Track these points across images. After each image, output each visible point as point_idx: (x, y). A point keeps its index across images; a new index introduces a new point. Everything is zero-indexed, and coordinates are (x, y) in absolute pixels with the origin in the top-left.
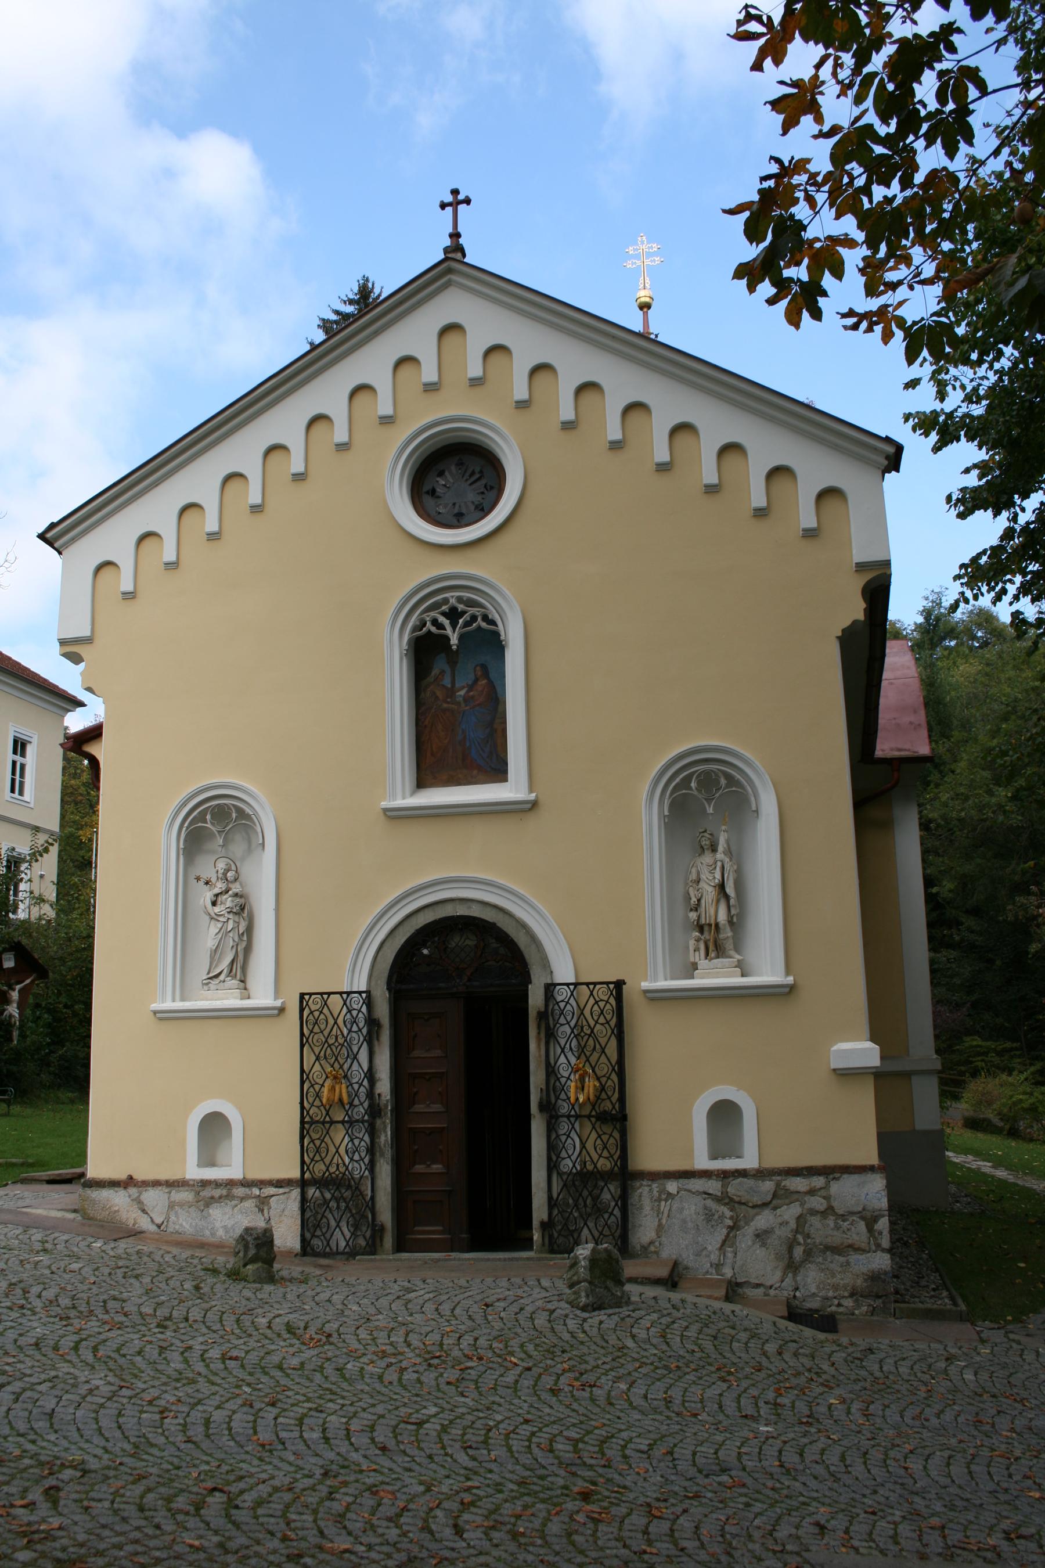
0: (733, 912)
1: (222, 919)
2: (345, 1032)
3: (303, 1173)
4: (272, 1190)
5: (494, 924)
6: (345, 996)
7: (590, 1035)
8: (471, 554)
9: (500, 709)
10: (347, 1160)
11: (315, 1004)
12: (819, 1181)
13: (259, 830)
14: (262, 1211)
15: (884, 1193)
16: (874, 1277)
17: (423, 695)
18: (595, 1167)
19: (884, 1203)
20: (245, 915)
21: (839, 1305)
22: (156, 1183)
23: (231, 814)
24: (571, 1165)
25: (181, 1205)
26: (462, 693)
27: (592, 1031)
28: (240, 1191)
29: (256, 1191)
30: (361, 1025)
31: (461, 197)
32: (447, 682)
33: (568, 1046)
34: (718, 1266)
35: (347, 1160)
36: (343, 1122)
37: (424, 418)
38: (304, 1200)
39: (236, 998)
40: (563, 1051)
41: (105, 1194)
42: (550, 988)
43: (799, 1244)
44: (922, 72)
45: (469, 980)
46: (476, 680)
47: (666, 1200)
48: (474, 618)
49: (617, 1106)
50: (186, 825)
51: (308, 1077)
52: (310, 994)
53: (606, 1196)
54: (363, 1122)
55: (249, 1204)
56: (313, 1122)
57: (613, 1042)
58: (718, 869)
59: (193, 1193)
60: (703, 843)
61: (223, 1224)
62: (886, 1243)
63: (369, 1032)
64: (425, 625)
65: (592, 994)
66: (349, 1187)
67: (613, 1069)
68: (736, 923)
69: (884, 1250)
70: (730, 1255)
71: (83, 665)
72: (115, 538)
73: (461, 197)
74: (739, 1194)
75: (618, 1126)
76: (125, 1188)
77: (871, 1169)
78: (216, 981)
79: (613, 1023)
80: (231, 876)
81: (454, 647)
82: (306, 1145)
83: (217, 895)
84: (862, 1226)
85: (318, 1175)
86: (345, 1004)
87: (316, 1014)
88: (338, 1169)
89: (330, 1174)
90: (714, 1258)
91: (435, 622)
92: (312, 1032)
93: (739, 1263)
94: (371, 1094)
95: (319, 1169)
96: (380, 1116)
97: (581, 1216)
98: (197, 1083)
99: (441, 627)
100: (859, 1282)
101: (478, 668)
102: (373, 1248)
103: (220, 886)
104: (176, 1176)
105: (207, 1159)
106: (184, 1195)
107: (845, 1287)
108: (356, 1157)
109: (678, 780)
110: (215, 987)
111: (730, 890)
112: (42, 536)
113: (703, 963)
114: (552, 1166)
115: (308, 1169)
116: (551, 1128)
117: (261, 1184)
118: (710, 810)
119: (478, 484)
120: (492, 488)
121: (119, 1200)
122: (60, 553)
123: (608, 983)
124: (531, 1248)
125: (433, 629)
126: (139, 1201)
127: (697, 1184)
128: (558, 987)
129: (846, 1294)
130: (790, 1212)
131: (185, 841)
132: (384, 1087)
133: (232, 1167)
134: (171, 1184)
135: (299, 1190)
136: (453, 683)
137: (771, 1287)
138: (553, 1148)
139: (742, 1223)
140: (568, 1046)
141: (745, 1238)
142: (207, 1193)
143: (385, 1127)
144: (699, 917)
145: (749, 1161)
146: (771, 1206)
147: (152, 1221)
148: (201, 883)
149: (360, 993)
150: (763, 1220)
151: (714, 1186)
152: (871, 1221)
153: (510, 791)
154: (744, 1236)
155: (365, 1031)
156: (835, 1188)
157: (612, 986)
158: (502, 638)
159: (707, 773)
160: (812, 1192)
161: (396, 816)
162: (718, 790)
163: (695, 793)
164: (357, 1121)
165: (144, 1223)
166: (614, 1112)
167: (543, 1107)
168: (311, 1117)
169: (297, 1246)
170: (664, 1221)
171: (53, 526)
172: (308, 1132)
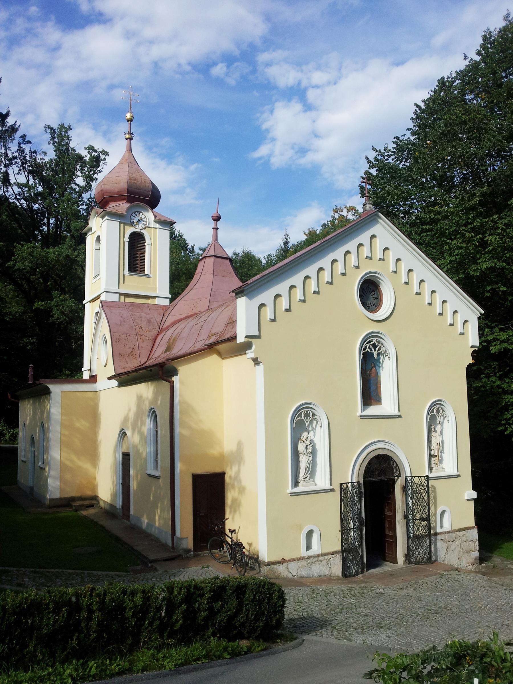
2: (414, 507)
4: (331, 556)
11: (344, 486)
22: (294, 560)
28: (321, 558)
29: (326, 557)
41: (275, 567)
44: (492, 354)
62: (478, 549)
77: (474, 527)
99: (371, 350)
104: (298, 556)
106: (303, 563)
117: (329, 554)
133: (316, 549)
142: (311, 560)
150: (453, 546)
169: (340, 575)
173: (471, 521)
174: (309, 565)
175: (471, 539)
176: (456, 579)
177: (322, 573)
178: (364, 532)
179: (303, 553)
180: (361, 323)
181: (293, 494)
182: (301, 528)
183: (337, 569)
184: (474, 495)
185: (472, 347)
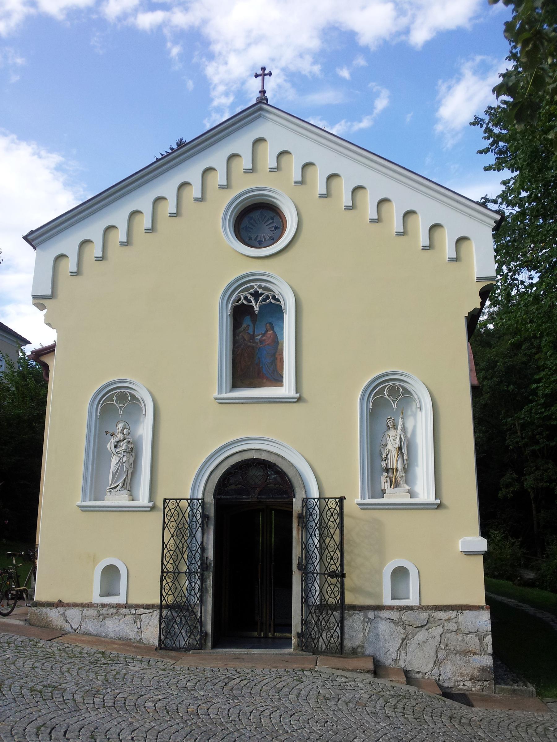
0: (406, 462)
1: (120, 455)
3: (161, 601)
5: (275, 464)
6: (189, 501)
7: (325, 528)
8: (266, 262)
9: (279, 347)
10: (187, 595)
11: (172, 505)
12: (453, 614)
13: (144, 407)
14: (135, 622)
15: (489, 621)
16: (483, 670)
17: (237, 338)
18: (327, 602)
19: (489, 628)
20: (133, 454)
21: (464, 685)
22: (75, 605)
23: (127, 397)
24: (314, 602)
25: (88, 617)
26: (259, 337)
27: (327, 526)
28: (124, 611)
30: (198, 517)
31: (266, 72)
32: (251, 331)
33: (313, 533)
34: (396, 661)
35: (187, 595)
36: (186, 573)
37: (245, 186)
38: (161, 616)
39: (126, 500)
40: (311, 536)
41: (44, 610)
42: (306, 501)
43: (442, 649)
45: (259, 494)
46: (267, 331)
47: (367, 622)
48: (268, 297)
49: (339, 569)
50: (101, 402)
51: (166, 547)
52: (170, 500)
53: (332, 619)
54: (197, 573)
55: (130, 618)
56: (168, 572)
57: (338, 531)
58: (398, 438)
59: (96, 611)
60: (389, 424)
61: (113, 629)
62: (490, 650)
63: (202, 522)
64: (240, 299)
65: (327, 504)
66: (188, 610)
67: (338, 547)
68: (406, 469)
69: (489, 654)
70: (403, 654)
71: (45, 311)
72: (67, 245)
73: (266, 72)
74: (409, 620)
75: (339, 580)
76: (56, 608)
77: (480, 608)
78: (115, 490)
79: (338, 521)
80: (128, 431)
81: (257, 312)
82: (164, 585)
83: (117, 442)
84: (477, 640)
85: (170, 602)
86: (189, 505)
87: (173, 511)
88: (182, 599)
89: (177, 602)
90: (394, 656)
91: (246, 298)
92: (169, 521)
93: (408, 660)
94: (202, 558)
95: (170, 599)
96: (207, 570)
97: (319, 630)
98: (104, 544)
100: (476, 672)
101: (268, 325)
102: (201, 646)
103: (120, 436)
105: (106, 593)
106: (92, 612)
107: (467, 674)
108: (193, 593)
109: (377, 389)
110: (114, 493)
111: (404, 450)
112: (25, 238)
113: (388, 490)
114: (305, 601)
115: (164, 599)
116: (305, 579)
117: (137, 607)
118: (394, 406)
119: (271, 226)
120: (279, 228)
121: (53, 615)
122: (35, 248)
123: (335, 498)
124: (289, 645)
125: (245, 302)
126: (64, 615)
127: (385, 614)
128: (309, 500)
129: (468, 679)
130: (437, 631)
131: (101, 411)
132: (210, 553)
134: (83, 606)
135: (159, 611)
136: (254, 332)
137: (426, 673)
138: (306, 591)
139: (410, 637)
140: (313, 533)
141: (412, 646)
142: (104, 611)
143: (209, 576)
144: (387, 464)
145: (413, 600)
146: (426, 627)
147: (72, 627)
148: (109, 435)
149: (198, 500)
150: (422, 635)
151: (395, 615)
152: (481, 639)
153: (287, 389)
154: (411, 644)
155: (200, 521)
156: (461, 618)
157: (337, 500)
158: (283, 308)
159: (394, 387)
160: (449, 620)
161: (222, 402)
162: (399, 396)
163: (387, 396)
164: (194, 572)
165: (67, 627)
166: (337, 572)
167: (300, 567)
168: (167, 570)
170: (366, 634)
171: (32, 232)
172: (165, 578)
173: (477, 594)
174: (101, 617)
175: (471, 628)
176: (177, 733)
177: (124, 635)
178: (210, 581)
179: (97, 599)
180: (238, 261)
181: (85, 509)
182: (95, 561)
183: (151, 632)
184: (482, 545)
185: (479, 279)
